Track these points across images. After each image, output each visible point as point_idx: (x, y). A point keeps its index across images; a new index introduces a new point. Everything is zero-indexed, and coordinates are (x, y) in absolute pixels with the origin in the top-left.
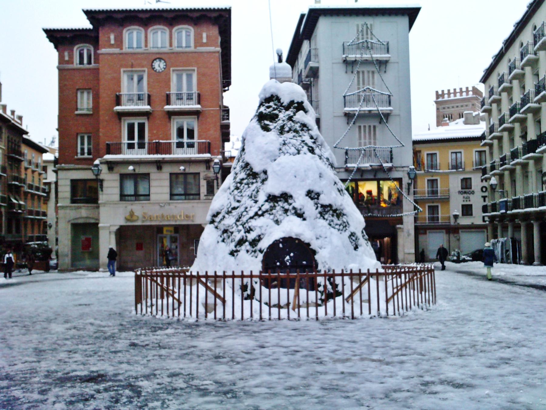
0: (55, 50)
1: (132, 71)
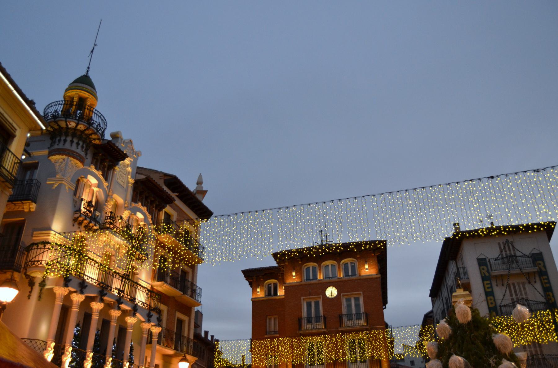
0: (251, 288)
1: (310, 298)
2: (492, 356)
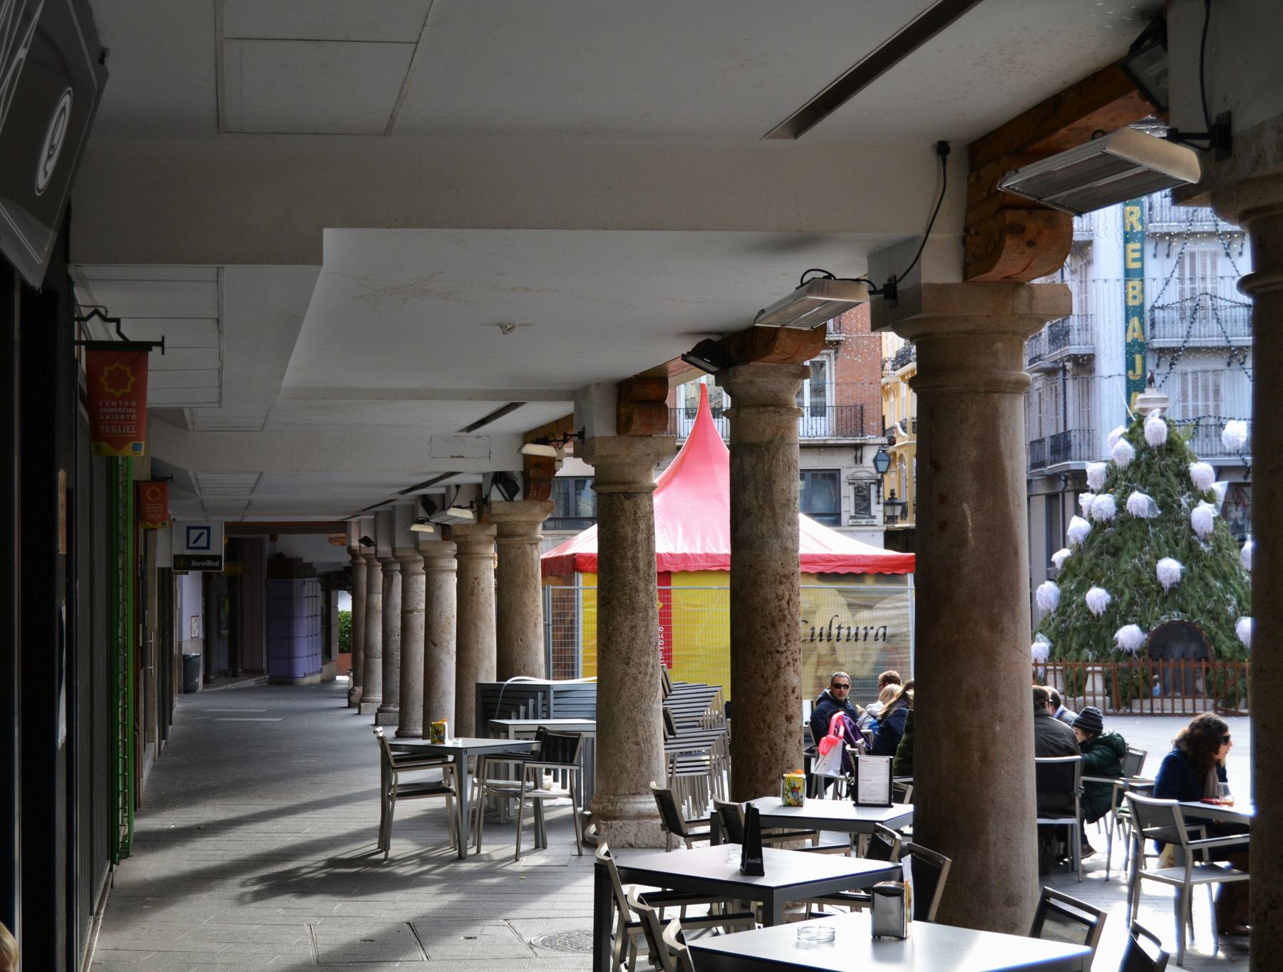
2: (1184, 493)
